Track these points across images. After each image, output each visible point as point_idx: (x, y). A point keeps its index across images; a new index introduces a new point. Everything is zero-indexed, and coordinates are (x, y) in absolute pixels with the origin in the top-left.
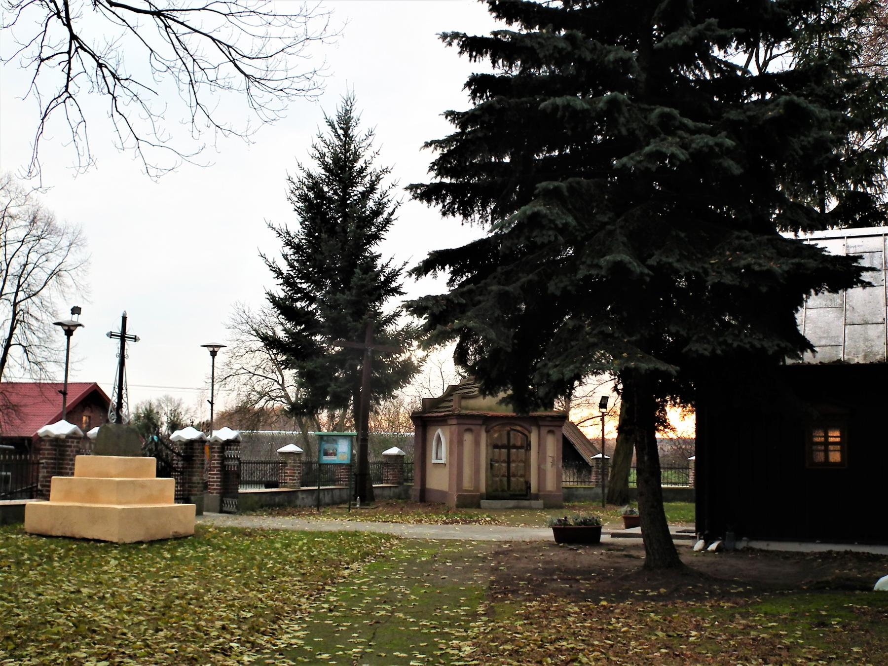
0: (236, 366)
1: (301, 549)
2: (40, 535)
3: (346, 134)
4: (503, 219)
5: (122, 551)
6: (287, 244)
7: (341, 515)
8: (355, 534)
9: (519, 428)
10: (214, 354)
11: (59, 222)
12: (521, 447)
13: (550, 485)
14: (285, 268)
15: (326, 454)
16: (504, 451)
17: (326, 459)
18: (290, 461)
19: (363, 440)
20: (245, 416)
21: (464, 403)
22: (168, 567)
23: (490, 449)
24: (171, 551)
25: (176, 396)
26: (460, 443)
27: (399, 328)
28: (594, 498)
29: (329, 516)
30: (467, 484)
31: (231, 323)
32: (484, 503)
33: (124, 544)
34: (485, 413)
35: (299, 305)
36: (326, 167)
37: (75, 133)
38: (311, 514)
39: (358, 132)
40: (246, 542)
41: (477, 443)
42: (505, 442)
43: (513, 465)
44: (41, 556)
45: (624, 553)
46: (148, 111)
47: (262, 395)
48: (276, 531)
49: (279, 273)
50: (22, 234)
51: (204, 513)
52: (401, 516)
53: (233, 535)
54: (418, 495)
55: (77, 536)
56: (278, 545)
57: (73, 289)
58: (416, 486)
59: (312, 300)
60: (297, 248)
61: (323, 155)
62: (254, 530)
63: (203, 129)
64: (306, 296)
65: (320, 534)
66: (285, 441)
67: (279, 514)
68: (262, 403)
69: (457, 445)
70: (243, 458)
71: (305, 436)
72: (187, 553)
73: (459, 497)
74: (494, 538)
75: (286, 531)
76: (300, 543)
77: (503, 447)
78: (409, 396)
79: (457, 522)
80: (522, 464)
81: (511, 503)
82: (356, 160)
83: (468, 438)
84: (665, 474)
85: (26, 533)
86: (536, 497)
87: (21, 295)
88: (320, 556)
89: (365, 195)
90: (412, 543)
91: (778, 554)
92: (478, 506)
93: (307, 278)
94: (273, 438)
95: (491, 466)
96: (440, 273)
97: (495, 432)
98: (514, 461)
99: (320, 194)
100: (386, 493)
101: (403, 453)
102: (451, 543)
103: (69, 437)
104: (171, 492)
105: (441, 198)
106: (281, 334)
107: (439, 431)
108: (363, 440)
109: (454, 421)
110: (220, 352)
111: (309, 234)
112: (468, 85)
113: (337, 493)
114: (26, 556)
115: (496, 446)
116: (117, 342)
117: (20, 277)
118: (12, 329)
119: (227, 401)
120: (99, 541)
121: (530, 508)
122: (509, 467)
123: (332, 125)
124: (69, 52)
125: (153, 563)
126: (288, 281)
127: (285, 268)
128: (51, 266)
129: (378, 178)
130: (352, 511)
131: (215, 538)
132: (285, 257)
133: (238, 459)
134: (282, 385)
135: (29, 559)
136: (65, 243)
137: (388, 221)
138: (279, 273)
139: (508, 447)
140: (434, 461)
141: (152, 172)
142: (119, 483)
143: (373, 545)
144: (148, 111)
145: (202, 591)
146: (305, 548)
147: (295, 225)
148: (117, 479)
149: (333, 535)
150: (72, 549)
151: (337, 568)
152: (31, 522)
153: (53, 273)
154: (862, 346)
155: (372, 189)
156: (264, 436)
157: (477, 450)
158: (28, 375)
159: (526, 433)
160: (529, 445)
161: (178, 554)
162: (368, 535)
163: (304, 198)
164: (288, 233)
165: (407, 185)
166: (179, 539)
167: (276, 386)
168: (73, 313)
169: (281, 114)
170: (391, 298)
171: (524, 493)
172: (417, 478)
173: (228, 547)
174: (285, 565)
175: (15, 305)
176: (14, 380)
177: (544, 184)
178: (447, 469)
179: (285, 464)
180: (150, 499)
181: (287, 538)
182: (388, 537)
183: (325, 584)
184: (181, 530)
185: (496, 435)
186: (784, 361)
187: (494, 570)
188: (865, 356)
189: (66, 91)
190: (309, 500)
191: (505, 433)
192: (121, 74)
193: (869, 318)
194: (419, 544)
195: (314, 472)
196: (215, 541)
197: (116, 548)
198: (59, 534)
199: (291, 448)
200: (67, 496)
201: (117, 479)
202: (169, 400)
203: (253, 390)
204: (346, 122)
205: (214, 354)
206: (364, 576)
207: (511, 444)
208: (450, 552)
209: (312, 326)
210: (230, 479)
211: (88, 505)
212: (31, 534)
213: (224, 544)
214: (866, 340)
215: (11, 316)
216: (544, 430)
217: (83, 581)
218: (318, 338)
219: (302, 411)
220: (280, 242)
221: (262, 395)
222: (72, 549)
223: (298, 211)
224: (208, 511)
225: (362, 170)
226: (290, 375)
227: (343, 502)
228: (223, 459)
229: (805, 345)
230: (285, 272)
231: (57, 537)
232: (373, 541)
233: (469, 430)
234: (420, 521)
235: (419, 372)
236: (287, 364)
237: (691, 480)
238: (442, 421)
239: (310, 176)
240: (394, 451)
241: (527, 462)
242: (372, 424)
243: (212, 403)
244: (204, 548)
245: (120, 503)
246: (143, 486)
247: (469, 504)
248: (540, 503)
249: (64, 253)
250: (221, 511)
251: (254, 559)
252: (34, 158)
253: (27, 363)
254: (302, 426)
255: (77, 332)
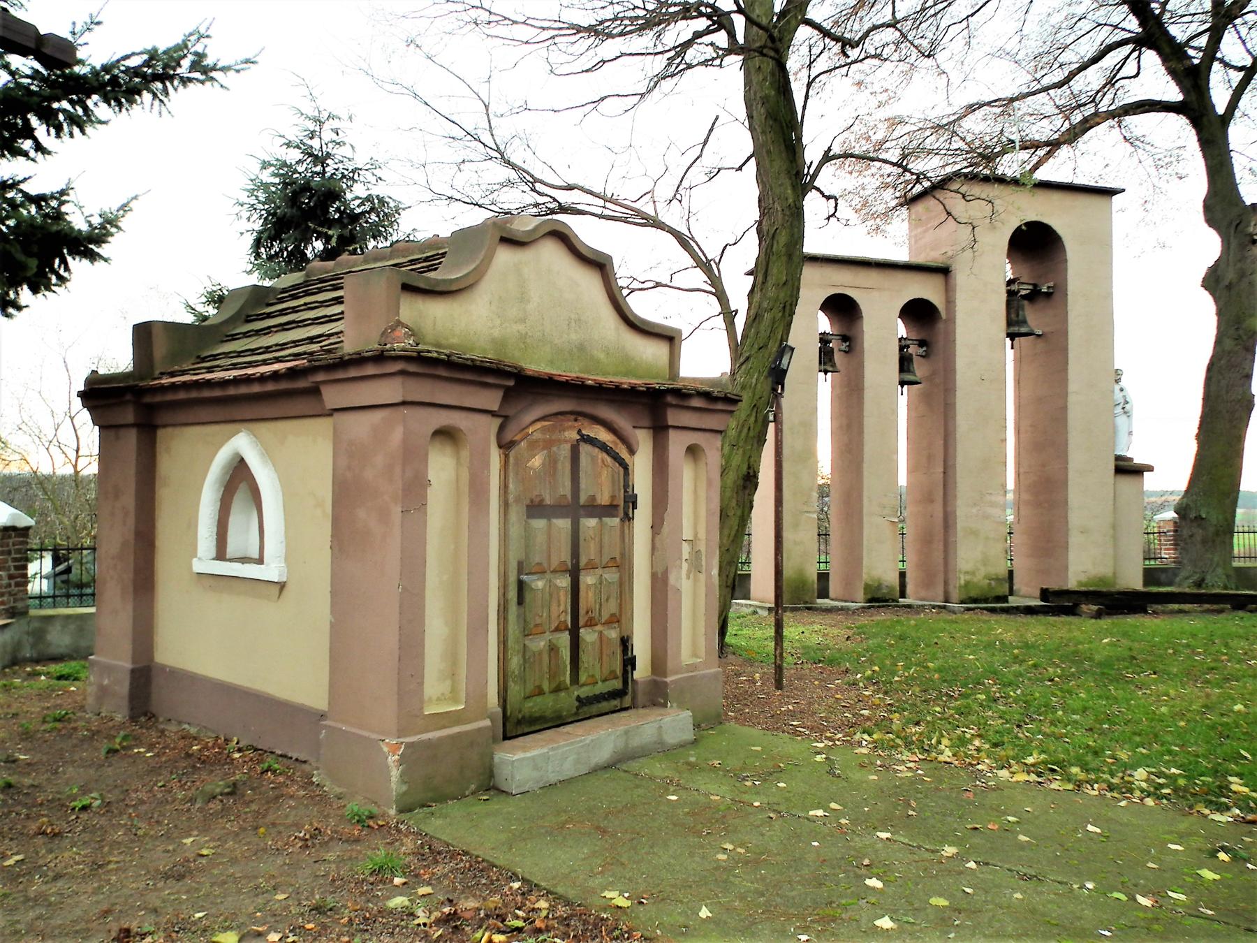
9: (603, 435)
12: (610, 510)
23: (516, 513)
42: (565, 488)
43: (588, 580)
54: (124, 688)
73: (413, 757)
77: (558, 510)
80: (612, 576)
97: (533, 446)
98: (592, 566)
101: (26, 521)
115: (536, 509)
139: (576, 508)
140: (204, 562)
159: (624, 454)
160: (632, 501)
171: (617, 684)
185: (537, 461)
191: (565, 451)
207: (583, 499)
241: (622, 564)
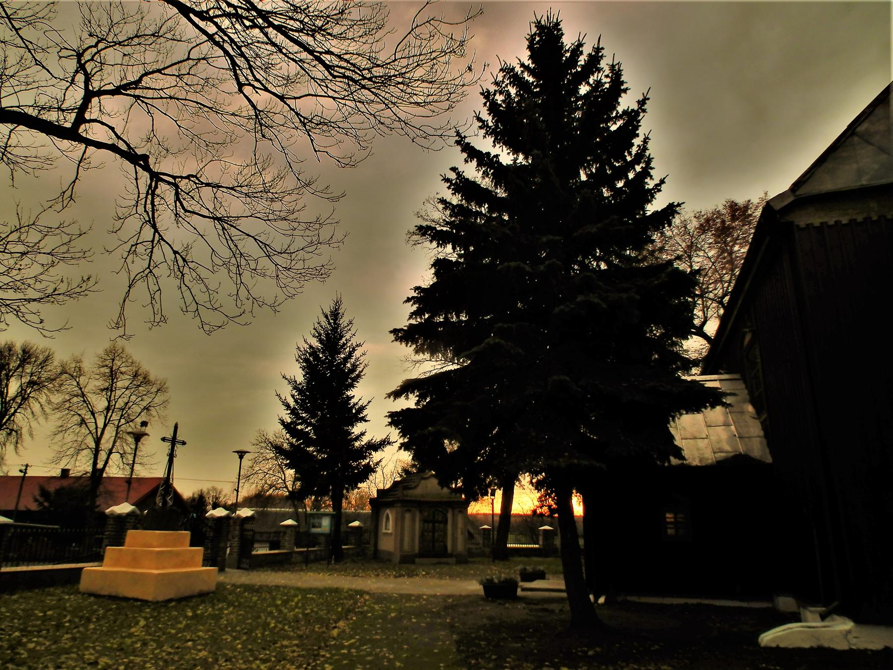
0: (257, 469)
1: (297, 606)
2: (91, 595)
3: (335, 323)
4: (35, 648)
5: (154, 609)
6: (294, 389)
7: (322, 570)
8: (337, 591)
10: (241, 457)
11: (152, 377)
13: (460, 547)
14: (292, 403)
15: (314, 526)
16: (431, 525)
17: (314, 530)
18: (289, 531)
19: (338, 518)
20: (258, 500)
21: (405, 492)
22: (188, 627)
24: (194, 609)
25: (219, 486)
26: (403, 518)
27: (363, 443)
28: (482, 555)
29: (314, 571)
30: (406, 547)
31: (255, 442)
32: (417, 560)
33: (157, 602)
34: (418, 499)
35: (299, 427)
36: (321, 341)
37: (153, 298)
38: (302, 570)
39: (343, 321)
40: (255, 599)
41: (413, 520)
43: (436, 534)
44: (81, 618)
45: (539, 607)
46: (207, 287)
47: (271, 486)
48: (277, 587)
49: (288, 406)
50: (127, 383)
51: (227, 569)
52: (363, 570)
53: (245, 592)
55: (121, 595)
56: (279, 602)
57: (157, 418)
58: (371, 548)
59: (309, 424)
60: (301, 392)
61: (320, 335)
62: (260, 587)
63: (245, 301)
64: (304, 421)
65: (310, 590)
66: (286, 516)
67: (279, 570)
68: (271, 491)
69: (400, 521)
70: (257, 530)
71: (296, 513)
72: (207, 610)
74: (439, 591)
75: (285, 587)
76: (296, 600)
78: (371, 487)
79: (404, 576)
81: (435, 560)
82: (341, 337)
83: (408, 516)
84: (141, 472)
85: (80, 593)
86: (451, 556)
87: (123, 421)
88: (313, 614)
89: (346, 360)
90: (380, 598)
91: (647, 604)
92: (413, 562)
93: (306, 410)
94: (276, 513)
95: (422, 535)
96: (411, 396)
99: (316, 357)
100: (350, 552)
102: (408, 597)
103: (129, 515)
104: (200, 558)
105: (414, 341)
106: (286, 446)
107: (388, 511)
108: (338, 518)
109: (399, 505)
110: (246, 456)
111: (308, 383)
112: (434, 265)
113: (319, 553)
114: (68, 618)
116: (168, 445)
117: (123, 410)
118: (115, 442)
119: (247, 490)
120: (136, 600)
121: (447, 564)
122: (433, 535)
123: (326, 317)
124: (153, 241)
125: (176, 620)
126: (293, 412)
127: (292, 403)
128: (144, 404)
129: (354, 350)
130: (330, 566)
131: (230, 594)
132: (293, 396)
133: (253, 531)
134: (284, 480)
135: (69, 621)
136: (154, 389)
137: (359, 376)
138: (288, 406)
140: (384, 531)
141: (207, 328)
142: (158, 552)
143: (351, 602)
144: (207, 287)
145: (210, 660)
146: (300, 605)
147: (300, 376)
148: (157, 549)
149: (320, 592)
150: (111, 610)
151: (327, 627)
152: (85, 584)
153: (145, 408)
154: (696, 454)
155: (350, 356)
156: (271, 512)
157: (413, 524)
158: (121, 472)
160: (447, 520)
161: (199, 612)
162: (347, 592)
163: (306, 360)
164: (296, 382)
165: (392, 329)
166: (203, 596)
167: (280, 481)
168: (142, 426)
169: (299, 290)
170: (359, 424)
172: (372, 542)
173: (240, 604)
174: (285, 625)
175: (118, 427)
176: (111, 475)
177: (500, 325)
178: (393, 537)
179: (285, 533)
180: (184, 564)
181: (286, 594)
182: (361, 593)
183: (320, 648)
184: (205, 588)
186: (669, 461)
187: (452, 626)
188: (701, 460)
189: (149, 268)
190: (300, 558)
192: (188, 258)
193: (697, 435)
194: (385, 599)
195: (303, 536)
196: (230, 597)
197: (149, 606)
198: (106, 593)
199: (290, 522)
200: (117, 562)
201: (157, 549)
202: (214, 489)
203: (266, 483)
204: (335, 315)
205: (241, 457)
206: (351, 637)
208: (411, 607)
209: (309, 442)
210: (246, 545)
211: (131, 570)
212: (84, 594)
213: (237, 601)
214: (698, 449)
215: (114, 434)
216: (456, 511)
217: (107, 647)
218: (311, 449)
219: (296, 497)
220: (290, 388)
221: (271, 486)
222: (111, 610)
223: (303, 368)
224: (230, 567)
225: (344, 344)
226: (290, 473)
227: (322, 559)
228: (243, 530)
229: (678, 452)
230: (292, 406)
231: (104, 596)
232: (351, 597)
233: (409, 511)
234: (378, 575)
235: (374, 472)
236: (289, 466)
237: (541, 543)
238: (390, 505)
239: (311, 347)
240: (356, 523)
242: (344, 504)
243: (238, 491)
244: (220, 606)
245: (157, 568)
246: (177, 554)
247: (407, 563)
248: (453, 560)
249: (153, 396)
250: (239, 568)
251: (259, 617)
252: (121, 314)
253: (121, 464)
254: (296, 507)
255: (143, 439)
